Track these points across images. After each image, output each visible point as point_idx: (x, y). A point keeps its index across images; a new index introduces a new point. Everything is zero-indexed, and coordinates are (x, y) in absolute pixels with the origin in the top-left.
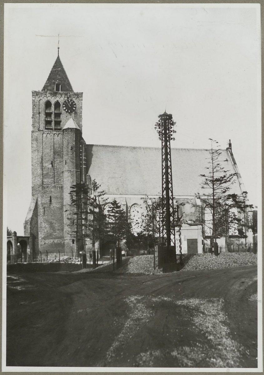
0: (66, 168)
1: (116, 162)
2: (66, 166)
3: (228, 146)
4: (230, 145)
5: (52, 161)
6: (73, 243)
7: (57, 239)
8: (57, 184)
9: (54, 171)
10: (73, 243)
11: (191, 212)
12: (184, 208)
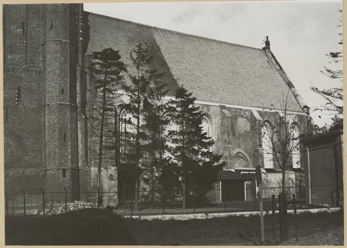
0: (52, 35)
1: (125, 42)
2: (52, 32)
3: (264, 45)
4: (268, 43)
5: (23, 23)
6: (64, 176)
7: (31, 168)
8: (31, 65)
9: (26, 41)
10: (64, 176)
11: (246, 131)
12: (236, 124)
